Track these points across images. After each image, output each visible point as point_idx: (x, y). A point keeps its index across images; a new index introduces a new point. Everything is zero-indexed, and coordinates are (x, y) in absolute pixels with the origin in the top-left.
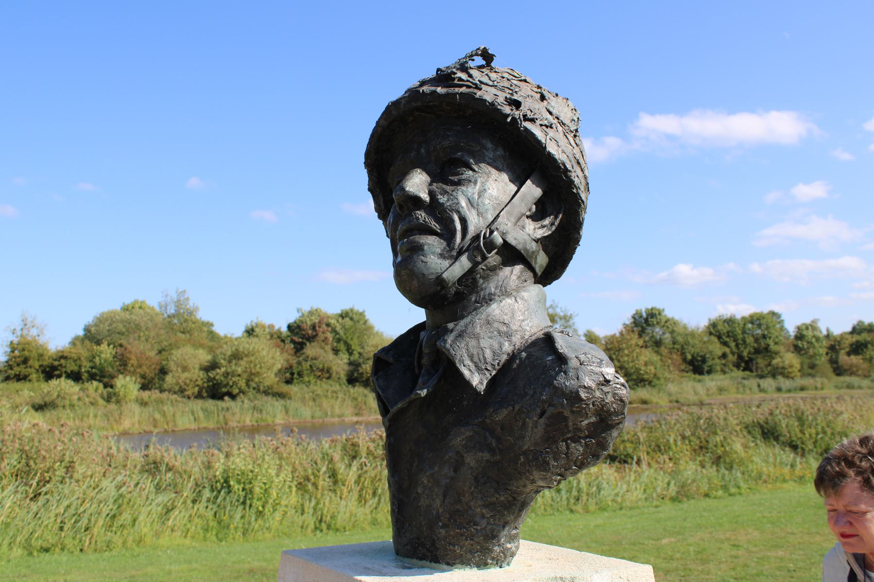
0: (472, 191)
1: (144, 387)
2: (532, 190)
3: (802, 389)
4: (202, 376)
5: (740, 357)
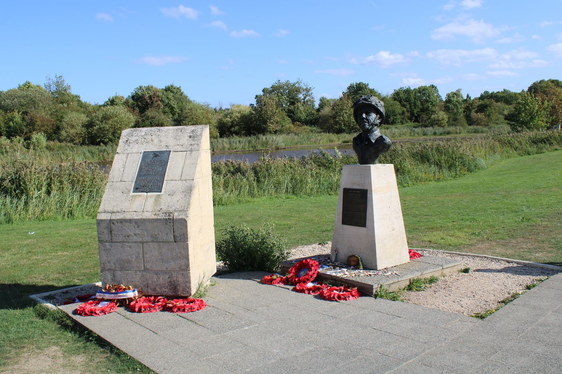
0: (371, 117)
1: (49, 138)
2: (378, 116)
3: (448, 133)
4: (84, 131)
5: (412, 114)
